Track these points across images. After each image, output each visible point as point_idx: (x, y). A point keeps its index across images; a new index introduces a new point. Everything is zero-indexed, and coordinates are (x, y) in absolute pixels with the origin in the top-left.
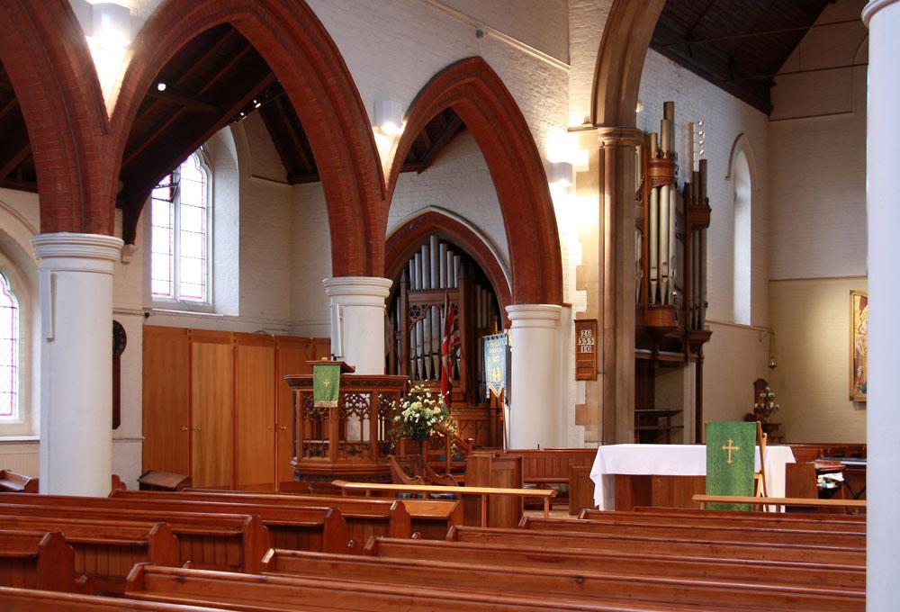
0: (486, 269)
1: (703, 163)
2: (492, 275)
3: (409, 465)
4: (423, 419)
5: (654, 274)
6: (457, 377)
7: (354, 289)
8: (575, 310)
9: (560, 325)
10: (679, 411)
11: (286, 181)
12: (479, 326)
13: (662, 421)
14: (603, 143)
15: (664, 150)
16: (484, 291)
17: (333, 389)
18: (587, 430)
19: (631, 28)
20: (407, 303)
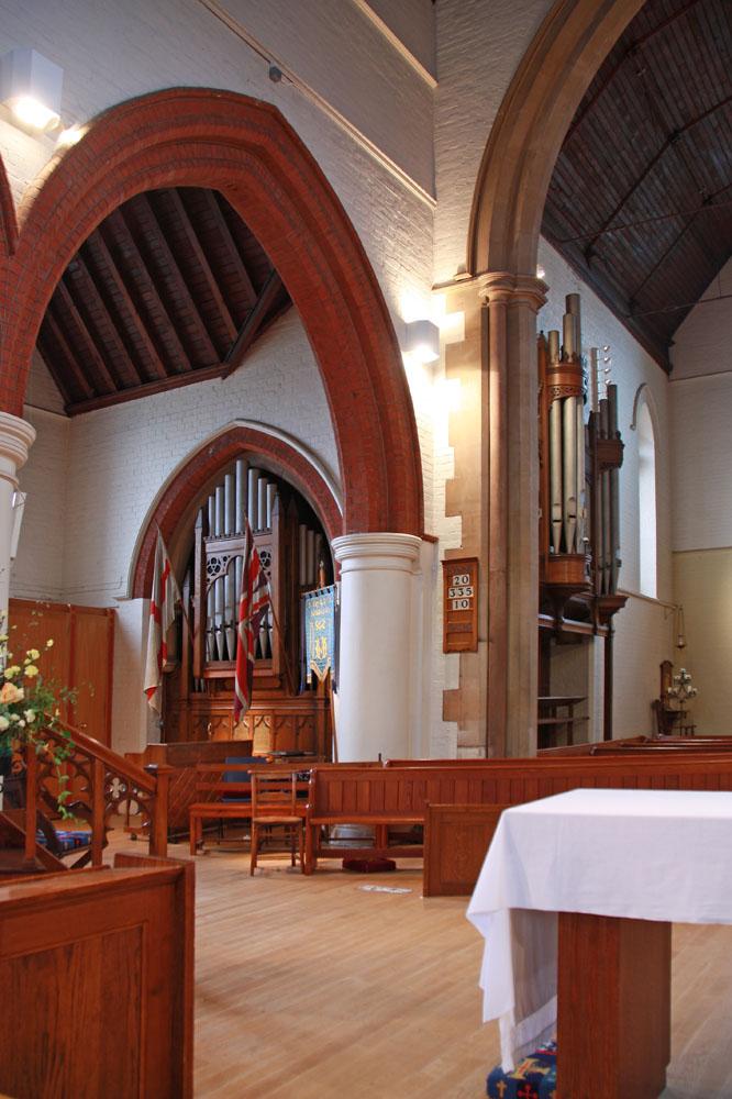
0: (312, 498)
1: (612, 389)
2: (320, 506)
5: (556, 513)
8: (444, 545)
9: (419, 568)
10: (579, 700)
11: (63, 412)
12: (303, 582)
13: (562, 711)
14: (487, 299)
15: (569, 350)
16: (311, 533)
18: (461, 728)
19: (527, 141)
20: (204, 554)
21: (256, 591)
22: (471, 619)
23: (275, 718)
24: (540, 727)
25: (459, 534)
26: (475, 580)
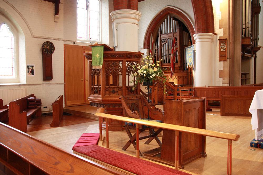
2: (188, 26)
3: (134, 102)
4: (148, 75)
5: (244, 26)
6: (177, 62)
7: (123, 15)
8: (219, 36)
9: (213, 41)
10: (248, 73)
12: (184, 44)
16: (186, 33)
17: (100, 59)
18: (223, 79)
20: (161, 38)
21: (175, 47)
22: (226, 53)
23: (178, 76)
24: (242, 80)
25: (223, 33)
26: (226, 44)
